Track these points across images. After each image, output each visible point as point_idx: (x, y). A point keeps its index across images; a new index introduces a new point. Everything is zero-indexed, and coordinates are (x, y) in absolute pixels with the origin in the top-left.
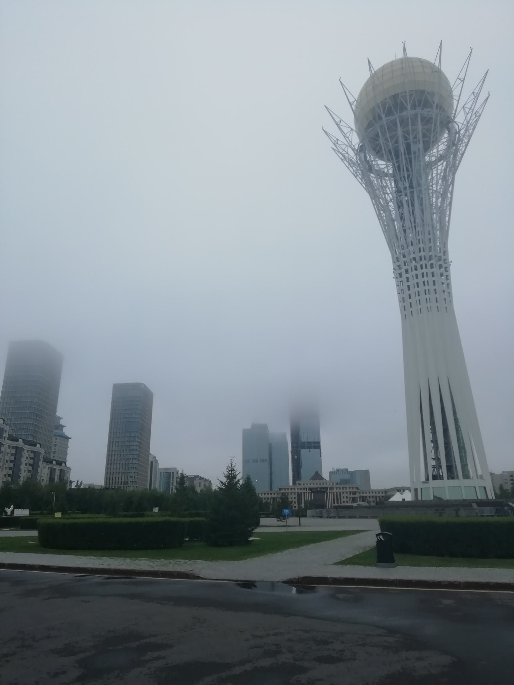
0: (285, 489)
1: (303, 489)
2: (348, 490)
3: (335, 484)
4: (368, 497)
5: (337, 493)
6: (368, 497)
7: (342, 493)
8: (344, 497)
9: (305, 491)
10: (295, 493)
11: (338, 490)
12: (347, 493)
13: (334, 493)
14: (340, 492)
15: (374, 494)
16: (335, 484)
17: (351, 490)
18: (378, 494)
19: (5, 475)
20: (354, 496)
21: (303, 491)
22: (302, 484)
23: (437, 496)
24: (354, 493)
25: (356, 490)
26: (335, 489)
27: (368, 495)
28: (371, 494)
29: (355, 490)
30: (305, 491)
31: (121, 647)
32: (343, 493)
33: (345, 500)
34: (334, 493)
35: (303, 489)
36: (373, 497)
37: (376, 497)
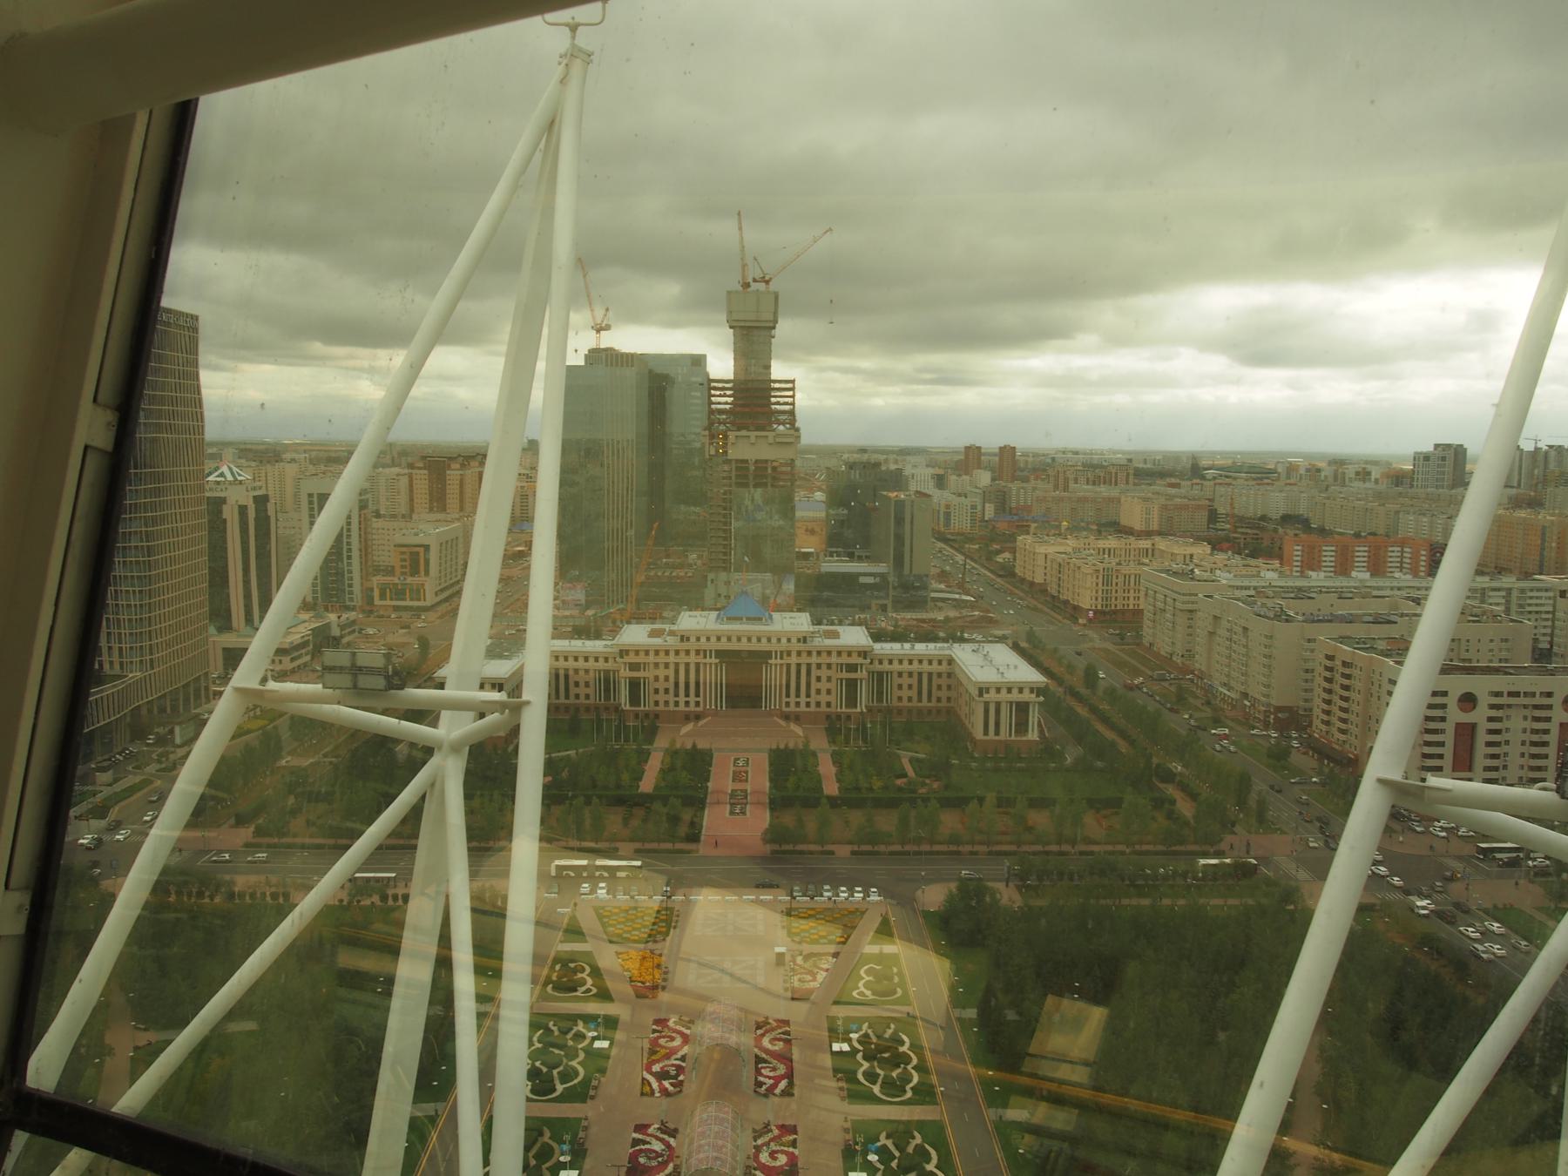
0: (637, 653)
1: (693, 653)
2: (834, 659)
3: (794, 640)
4: (895, 675)
5: (799, 665)
6: (895, 675)
7: (814, 667)
8: (819, 679)
9: (700, 659)
10: (667, 666)
11: (804, 660)
12: (829, 666)
13: (789, 665)
14: (809, 665)
15: (915, 667)
16: (794, 640)
17: (845, 660)
18: (925, 667)
19: (1522, 767)
20: (852, 676)
21: (692, 659)
22: (693, 639)
23: (187, 817)
24: (852, 668)
25: (860, 660)
26: (794, 654)
27: (896, 667)
28: (906, 666)
29: (855, 660)
30: (700, 659)
31: (584, 862)
32: (819, 666)
33: (824, 686)
34: (789, 665)
35: (693, 653)
36: (910, 674)
37: (920, 674)
